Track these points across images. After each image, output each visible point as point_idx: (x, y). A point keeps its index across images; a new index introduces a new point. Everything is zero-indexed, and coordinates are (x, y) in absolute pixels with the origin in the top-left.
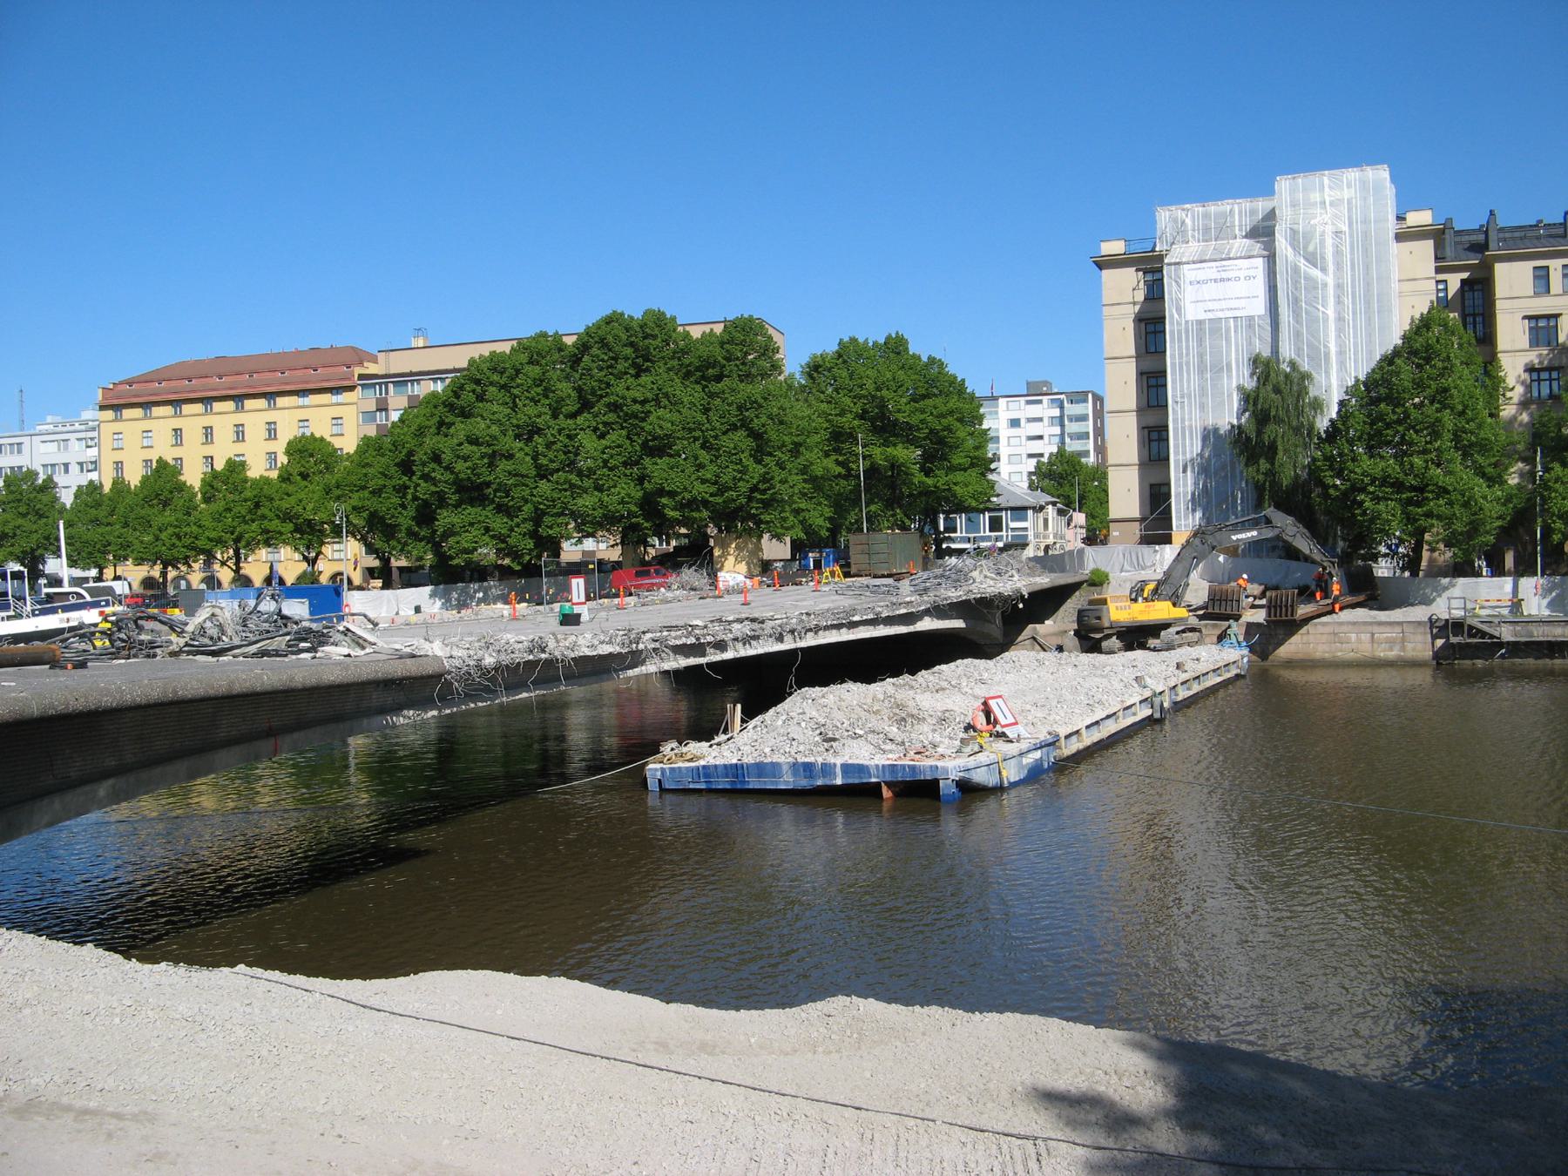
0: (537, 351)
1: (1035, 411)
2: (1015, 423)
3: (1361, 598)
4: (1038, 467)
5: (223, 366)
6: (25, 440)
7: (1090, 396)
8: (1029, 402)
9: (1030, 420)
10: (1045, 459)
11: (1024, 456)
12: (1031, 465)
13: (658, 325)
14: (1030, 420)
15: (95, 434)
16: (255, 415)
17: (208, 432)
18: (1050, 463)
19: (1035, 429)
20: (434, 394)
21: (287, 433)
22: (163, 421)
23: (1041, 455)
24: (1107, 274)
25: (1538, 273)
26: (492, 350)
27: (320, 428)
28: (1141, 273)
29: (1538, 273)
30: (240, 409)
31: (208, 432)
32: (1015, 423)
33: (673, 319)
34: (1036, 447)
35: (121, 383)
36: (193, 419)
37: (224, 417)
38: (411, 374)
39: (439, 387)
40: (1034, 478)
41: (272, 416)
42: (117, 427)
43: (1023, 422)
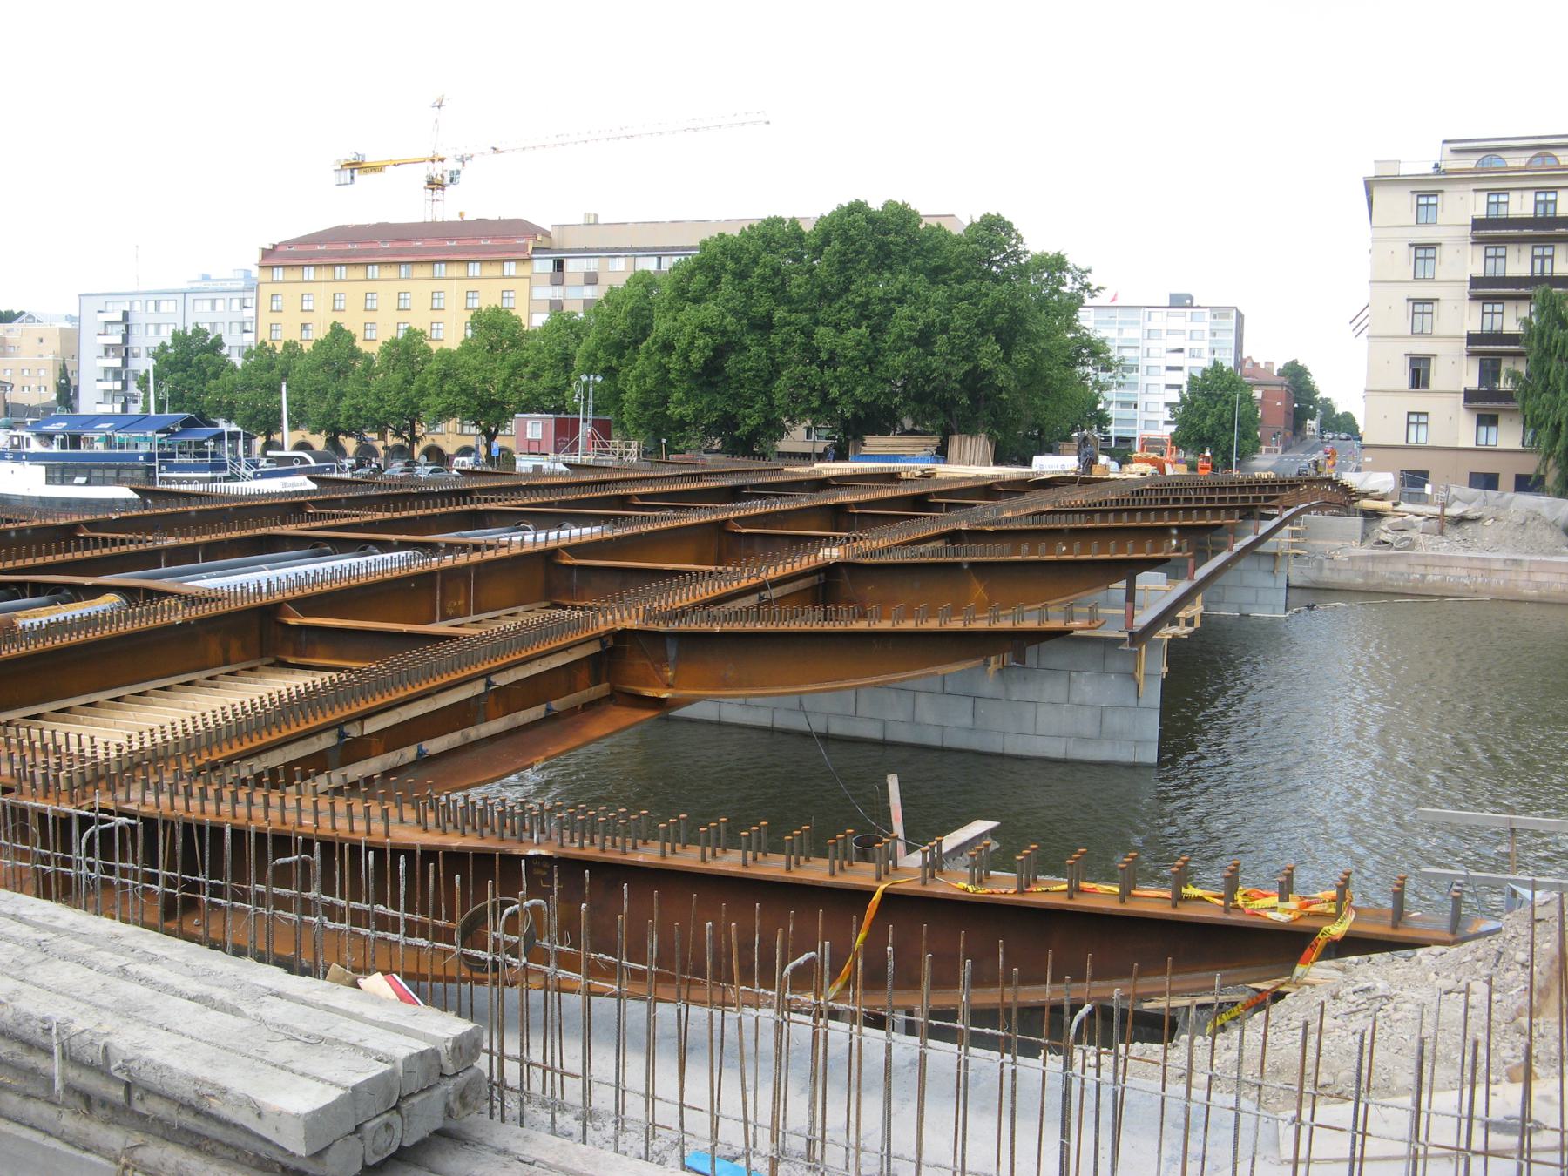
11: (1163, 369)
13: (899, 219)
28: (1415, 196)
39: (668, 263)
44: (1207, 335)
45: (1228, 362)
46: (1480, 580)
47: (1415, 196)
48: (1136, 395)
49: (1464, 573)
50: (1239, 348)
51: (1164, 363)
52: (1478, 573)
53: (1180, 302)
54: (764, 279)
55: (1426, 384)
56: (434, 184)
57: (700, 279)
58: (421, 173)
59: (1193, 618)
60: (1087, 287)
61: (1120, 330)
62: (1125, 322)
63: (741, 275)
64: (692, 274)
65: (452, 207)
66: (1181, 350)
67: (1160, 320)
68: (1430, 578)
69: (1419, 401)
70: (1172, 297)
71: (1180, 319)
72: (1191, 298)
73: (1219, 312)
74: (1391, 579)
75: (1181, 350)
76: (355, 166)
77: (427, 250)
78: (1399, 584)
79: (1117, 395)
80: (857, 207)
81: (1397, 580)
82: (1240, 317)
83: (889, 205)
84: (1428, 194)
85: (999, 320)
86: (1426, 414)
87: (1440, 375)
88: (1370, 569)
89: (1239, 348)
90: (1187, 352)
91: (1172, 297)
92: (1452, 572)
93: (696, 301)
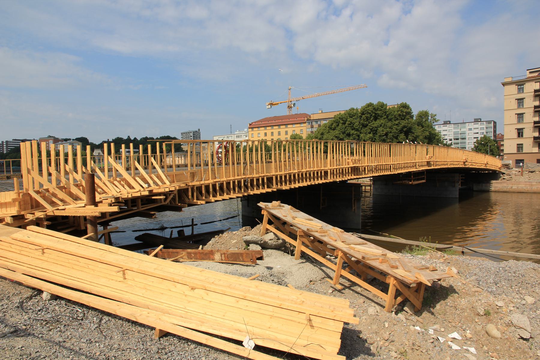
0: (351, 113)
1: (476, 126)
2: (470, 129)
3: (352, 272)
4: (477, 140)
5: (276, 118)
6: (233, 135)
7: (493, 122)
8: (474, 124)
9: (474, 129)
10: (479, 139)
11: (473, 138)
12: (475, 140)
13: (382, 106)
14: (474, 129)
15: (248, 134)
16: (283, 129)
17: (272, 133)
18: (481, 140)
19: (476, 131)
20: (325, 124)
21: (290, 133)
22: (262, 131)
23: (478, 138)
24: (506, 87)
25: (356, 174)
26: (335, 115)
27: (298, 131)
28: (517, 86)
29: (356, 174)
30: (286, 127)
31: (272, 133)
32: (470, 129)
33: (386, 104)
34: (476, 136)
35: (253, 122)
36: (269, 130)
37: (276, 130)
38: (319, 119)
39: (327, 121)
40: (475, 144)
41: (286, 129)
42: (252, 132)
43: (473, 129)
44: (485, 128)
45: (491, 135)
46: (529, 187)
47: (517, 86)
48: (465, 145)
49: (523, 186)
50: (495, 131)
51: (473, 137)
52: (528, 186)
53: (477, 121)
54: (349, 124)
55: (522, 136)
56: (290, 107)
57: (335, 124)
58: (286, 105)
59: (151, 186)
60: (435, 119)
61: (460, 129)
62: (462, 127)
63: (344, 123)
64: (332, 124)
65: (294, 111)
66: (478, 133)
67: (472, 126)
68: (514, 187)
69: (520, 141)
70: (475, 119)
71: (478, 125)
72: (480, 119)
73: (489, 122)
74: (502, 188)
75: (478, 133)
76: (271, 104)
77: (271, 123)
78: (505, 189)
79: (460, 145)
80: (370, 105)
81: (504, 188)
82: (495, 123)
83: (379, 102)
84: (521, 85)
85: (405, 129)
86: (522, 144)
87: (526, 133)
88: (496, 186)
89: (495, 131)
90: (479, 133)
91: (475, 119)
92: (520, 186)
93: (334, 130)
